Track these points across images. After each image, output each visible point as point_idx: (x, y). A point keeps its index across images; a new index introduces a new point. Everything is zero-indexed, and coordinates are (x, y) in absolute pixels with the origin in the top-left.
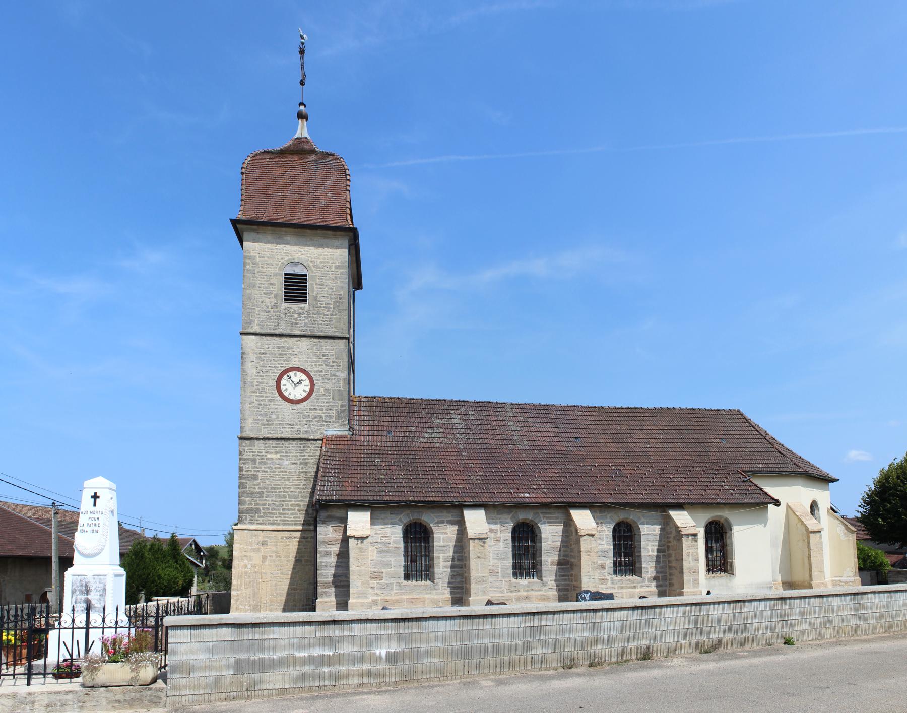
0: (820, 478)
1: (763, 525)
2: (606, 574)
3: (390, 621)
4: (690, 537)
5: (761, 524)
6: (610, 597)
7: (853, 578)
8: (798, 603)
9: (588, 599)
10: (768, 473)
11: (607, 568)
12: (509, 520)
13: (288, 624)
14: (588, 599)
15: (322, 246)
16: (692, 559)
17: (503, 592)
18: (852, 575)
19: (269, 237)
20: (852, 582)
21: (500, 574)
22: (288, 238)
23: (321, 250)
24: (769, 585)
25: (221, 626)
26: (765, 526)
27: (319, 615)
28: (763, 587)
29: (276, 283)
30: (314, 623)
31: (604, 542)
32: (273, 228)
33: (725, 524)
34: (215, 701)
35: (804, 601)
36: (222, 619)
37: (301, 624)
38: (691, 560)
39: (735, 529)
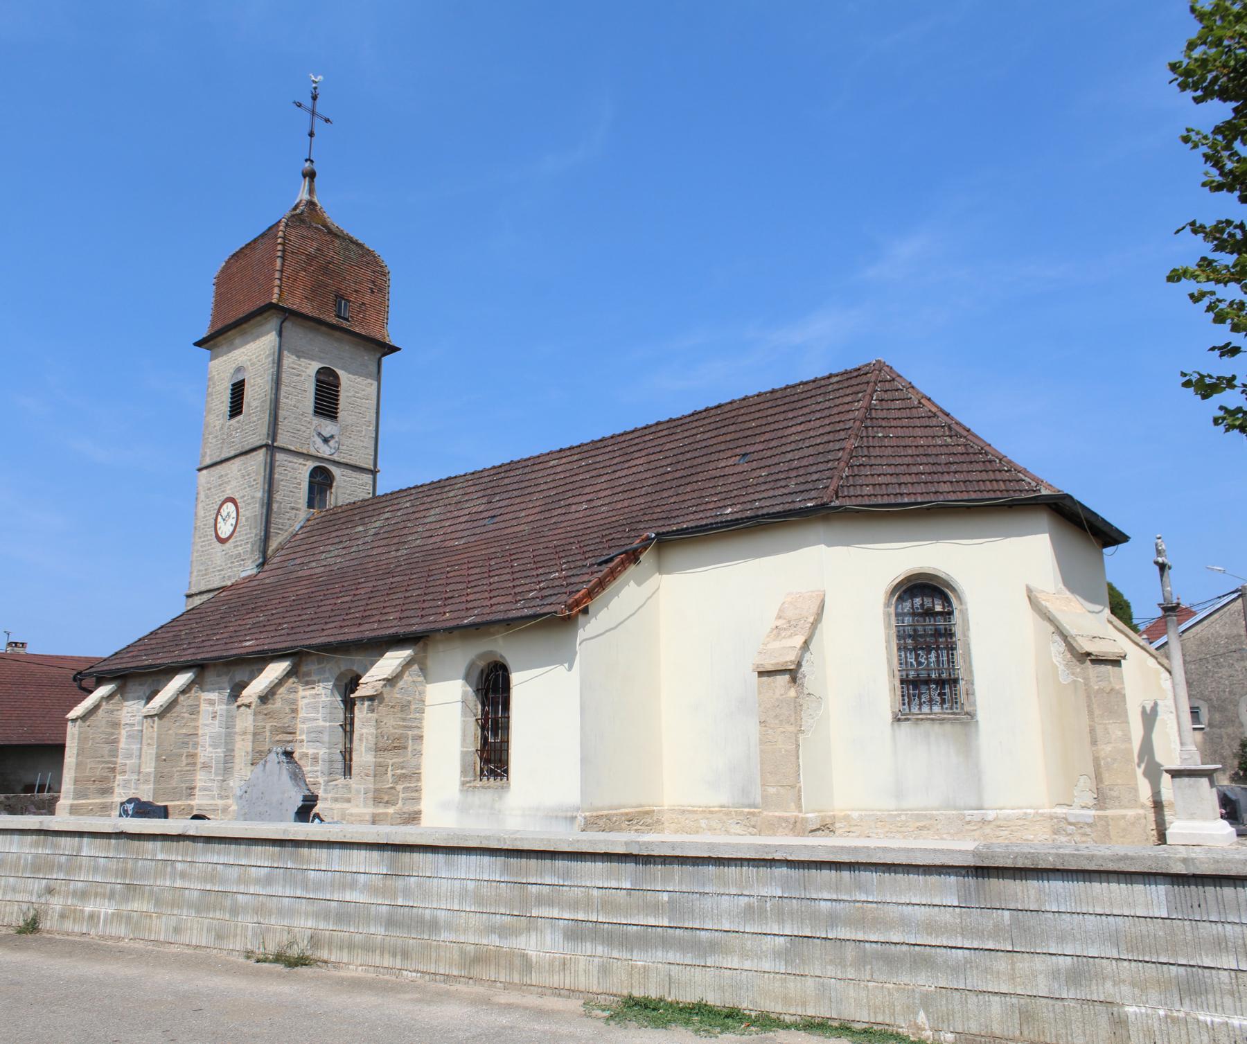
0: (969, 507)
1: (566, 665)
2: (319, 773)
3: (114, 836)
4: (367, 703)
5: (562, 665)
6: (164, 813)
7: (1093, 812)
8: (1193, 893)
9: (130, 813)
10: (727, 526)
11: (320, 762)
12: (226, 685)
13: (1185, 879)
14: (130, 813)
15: (258, 337)
16: (366, 747)
17: (213, 798)
18: (1091, 802)
19: (225, 348)
20: (1090, 825)
21: (213, 770)
22: (237, 341)
23: (257, 342)
24: (569, 814)
25: (1087, 876)
26: (570, 669)
27: (60, 820)
28: (557, 817)
29: (315, 366)
30: (524, 854)
31: (320, 715)
32: (238, 329)
33: (476, 674)
34: (440, 982)
35: (757, 873)
36: (613, 843)
37: (539, 854)
38: (363, 749)
39: (516, 678)
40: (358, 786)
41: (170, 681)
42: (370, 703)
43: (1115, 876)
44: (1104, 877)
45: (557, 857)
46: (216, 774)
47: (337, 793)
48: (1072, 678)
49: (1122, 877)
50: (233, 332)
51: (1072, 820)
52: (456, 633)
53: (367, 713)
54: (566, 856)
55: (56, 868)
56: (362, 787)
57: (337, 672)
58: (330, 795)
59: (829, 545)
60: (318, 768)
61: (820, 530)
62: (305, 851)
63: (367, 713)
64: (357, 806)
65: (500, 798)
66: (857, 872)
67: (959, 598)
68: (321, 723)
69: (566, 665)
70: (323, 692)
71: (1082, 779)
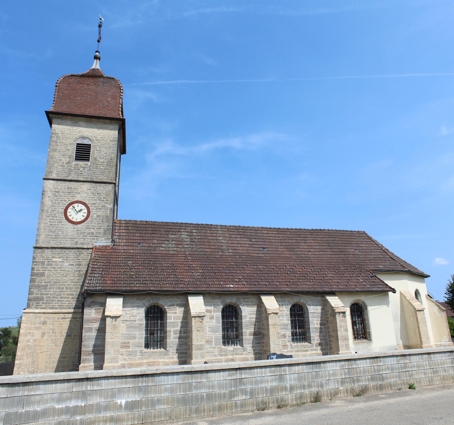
1: (387, 305)
2: (287, 341)
4: (341, 314)
7: (448, 343)
11: (287, 337)
12: (220, 303)
15: (102, 128)
16: (344, 329)
17: (215, 356)
18: (447, 341)
21: (213, 343)
23: (101, 131)
26: (388, 306)
31: (285, 318)
33: (363, 305)
38: (343, 330)
39: (369, 308)
40: (343, 343)
41: (262, 300)
42: (343, 314)
43: (166, 374)
44: (166, 374)
45: (50, 383)
46: (216, 344)
47: (298, 348)
48: (440, 315)
49: (172, 374)
50: (84, 118)
51: (442, 345)
52: (363, 293)
53: (342, 318)
54: (5, 385)
55: (395, 377)
56: (344, 344)
57: (148, 304)
58: (294, 350)
59: (408, 280)
60: (286, 339)
61: (406, 276)
62: (157, 378)
63: (342, 318)
64: (343, 350)
65: (370, 345)
66: (111, 380)
67: (420, 296)
68: (286, 322)
69: (387, 305)
70: (286, 309)
71: (444, 336)
